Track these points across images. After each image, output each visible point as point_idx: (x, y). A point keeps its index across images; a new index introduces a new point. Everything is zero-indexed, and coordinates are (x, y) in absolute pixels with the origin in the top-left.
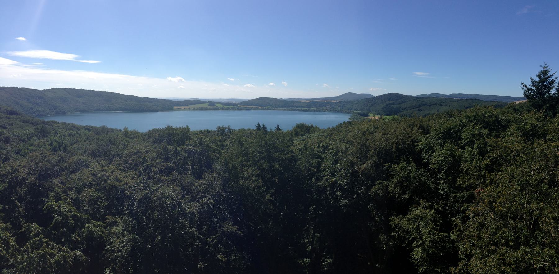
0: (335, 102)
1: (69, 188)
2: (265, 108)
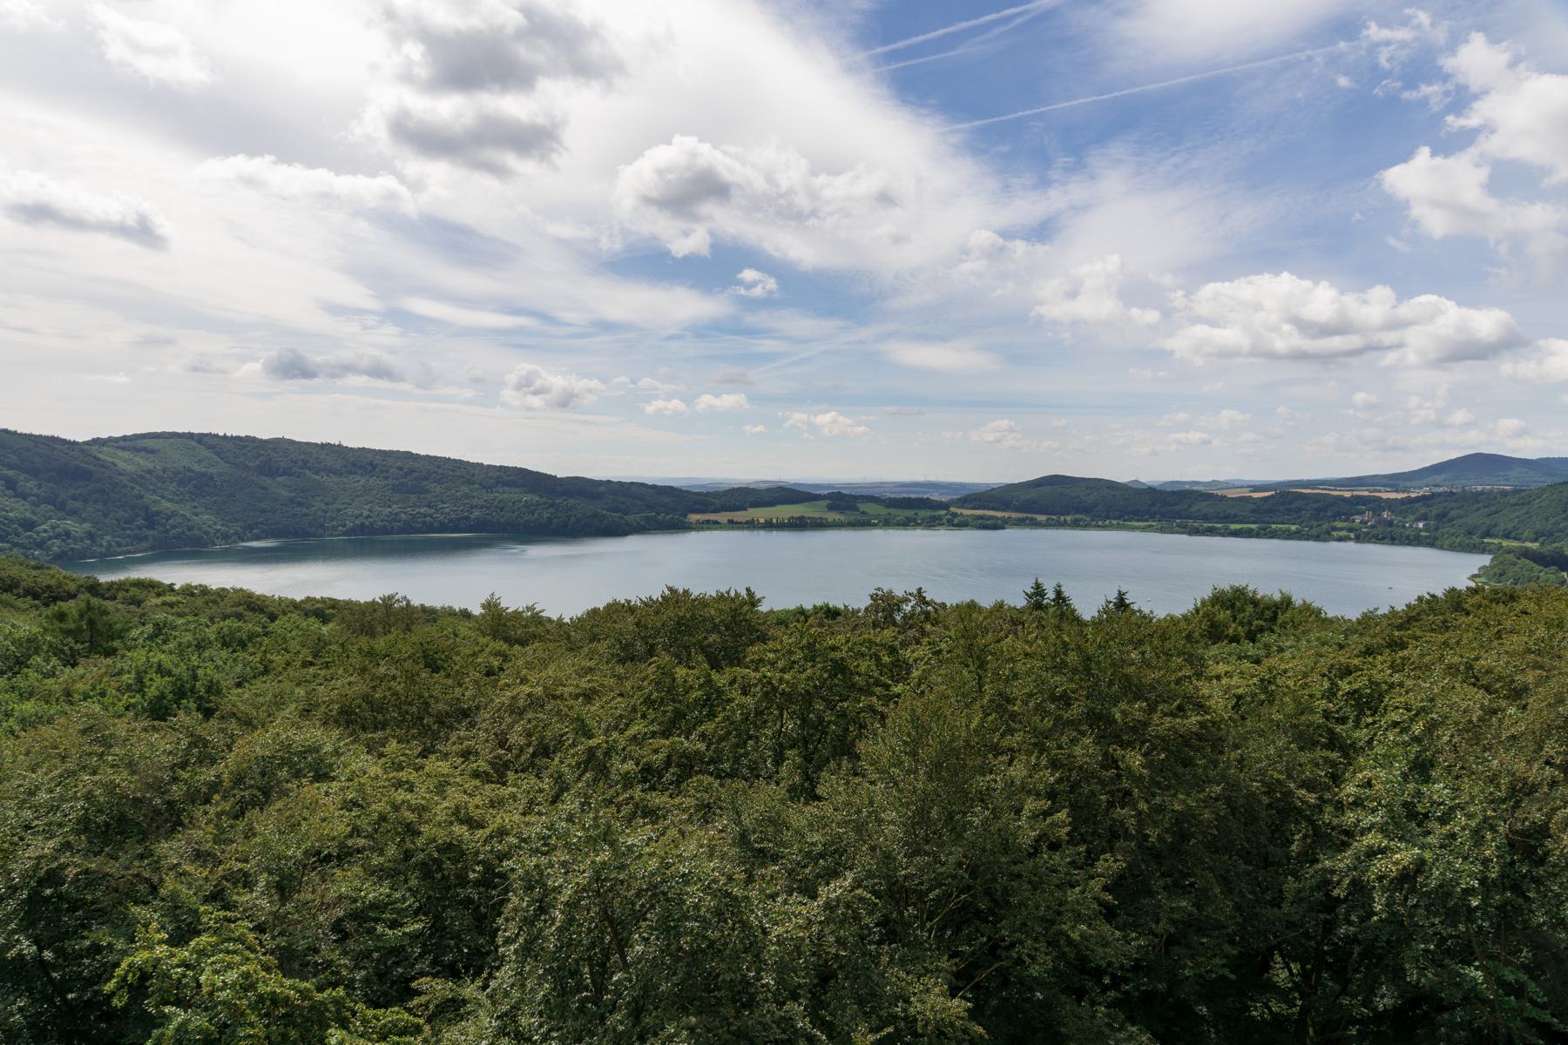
0: (1400, 496)
1: (230, 877)
2: (1062, 518)
